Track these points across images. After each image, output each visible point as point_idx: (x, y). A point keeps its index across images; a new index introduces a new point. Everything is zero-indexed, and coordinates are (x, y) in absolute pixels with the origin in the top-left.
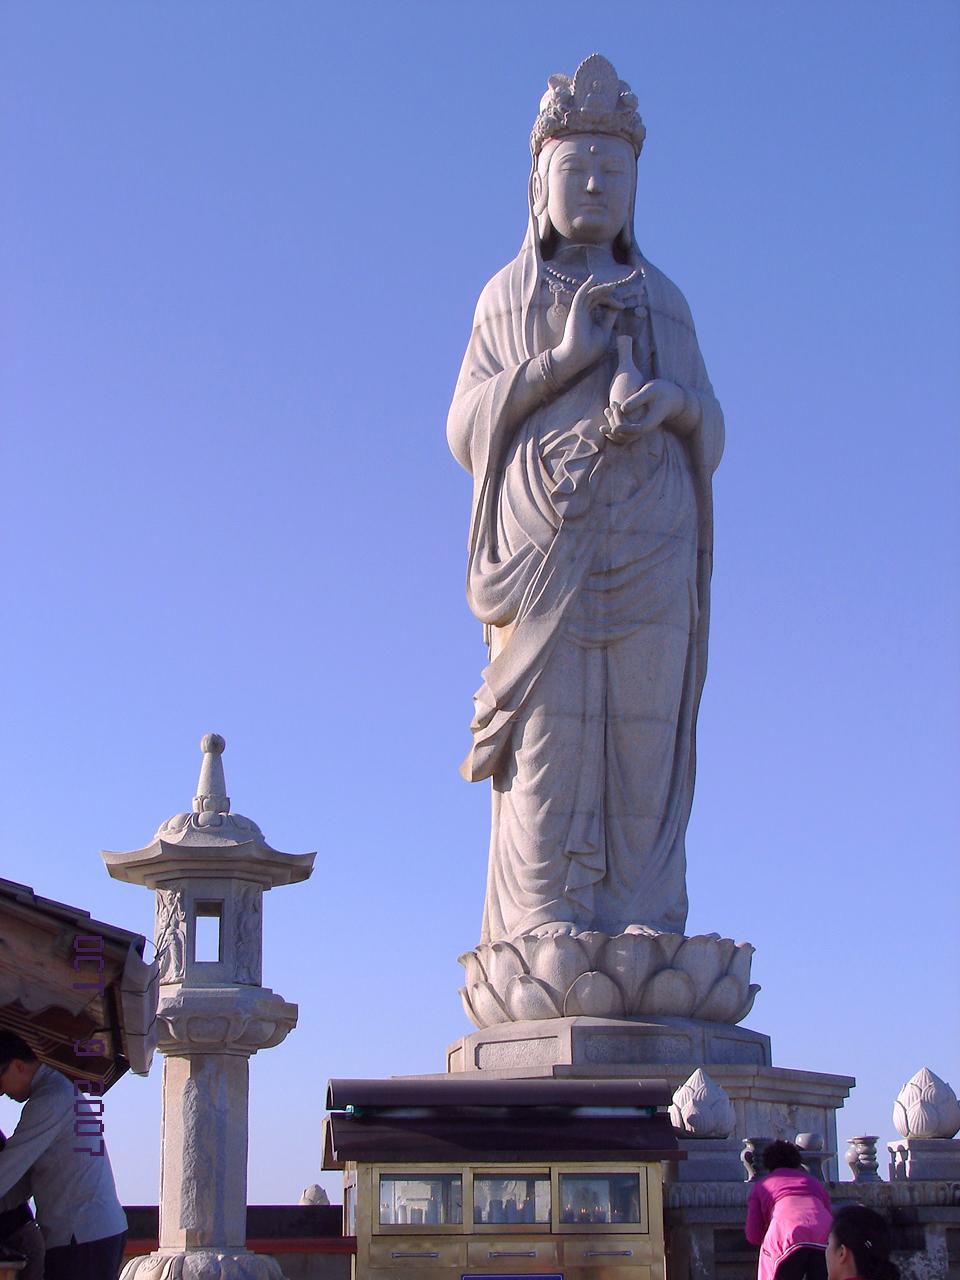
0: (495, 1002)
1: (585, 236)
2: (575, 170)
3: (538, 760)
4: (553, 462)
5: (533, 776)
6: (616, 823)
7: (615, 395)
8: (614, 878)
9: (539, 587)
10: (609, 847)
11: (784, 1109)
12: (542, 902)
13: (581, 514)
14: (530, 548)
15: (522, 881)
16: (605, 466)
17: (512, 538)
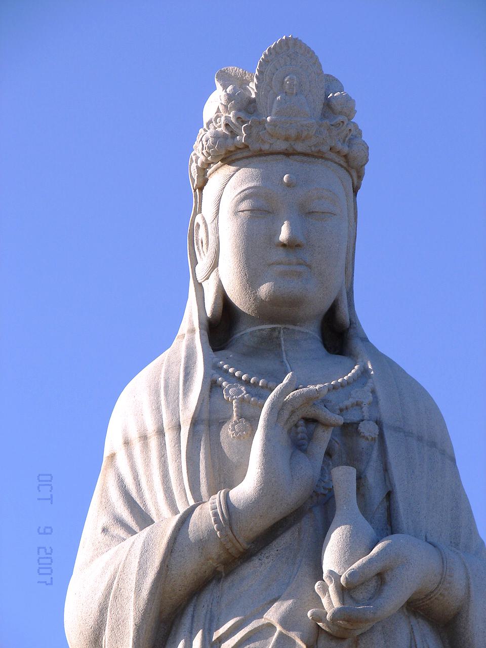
1: (278, 313)
2: (259, 212)
7: (331, 559)
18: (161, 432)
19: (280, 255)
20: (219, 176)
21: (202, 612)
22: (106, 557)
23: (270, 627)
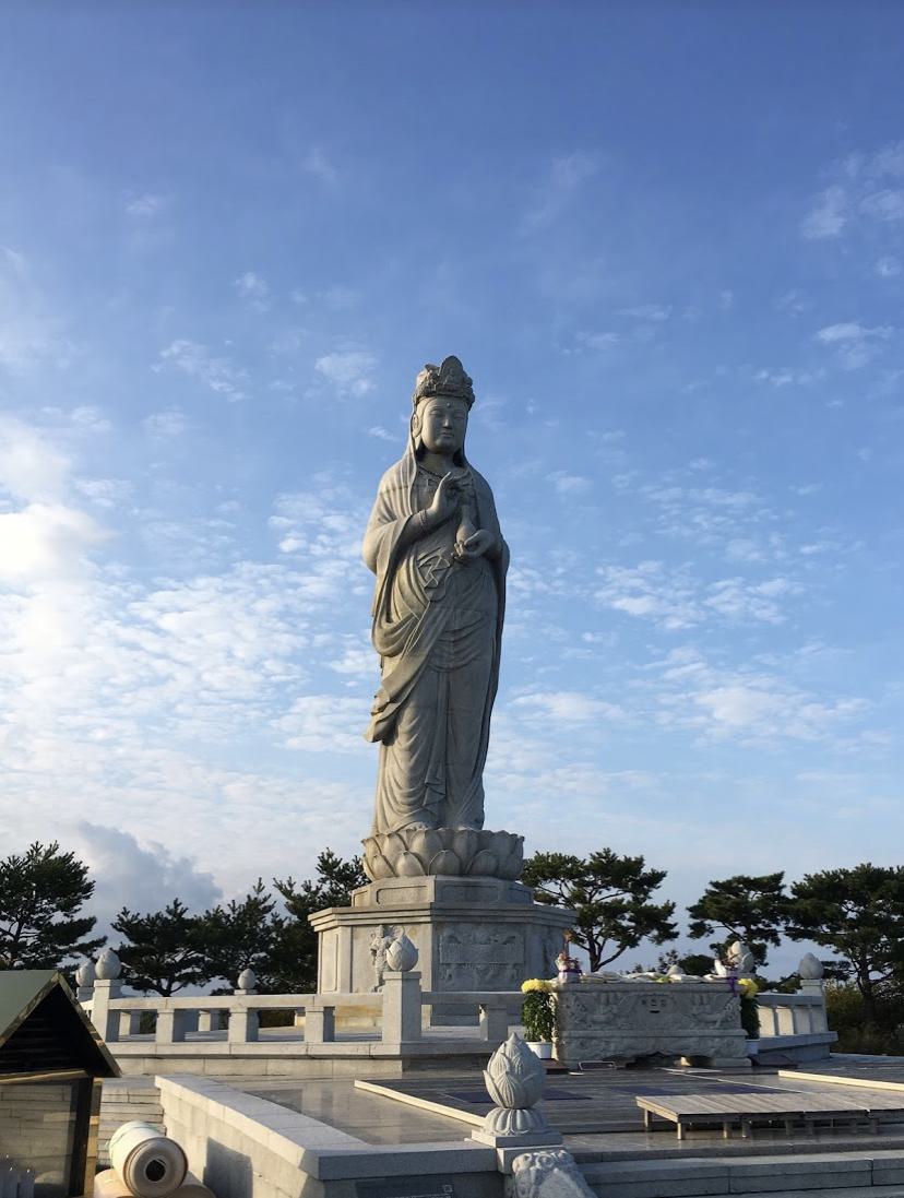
0: (387, 867)
1: (441, 451)
2: (438, 414)
3: (411, 732)
4: (425, 569)
5: (408, 740)
6: (451, 767)
7: (459, 536)
8: (450, 799)
9: (432, 638)
10: (448, 782)
11: (546, 930)
12: (411, 810)
13: (437, 595)
14: (412, 615)
15: (399, 799)
16: (454, 573)
17: (401, 610)
18: (394, 490)
19: (444, 431)
20: (423, 402)
21: (414, 550)
22: (378, 530)
23: (437, 557)
